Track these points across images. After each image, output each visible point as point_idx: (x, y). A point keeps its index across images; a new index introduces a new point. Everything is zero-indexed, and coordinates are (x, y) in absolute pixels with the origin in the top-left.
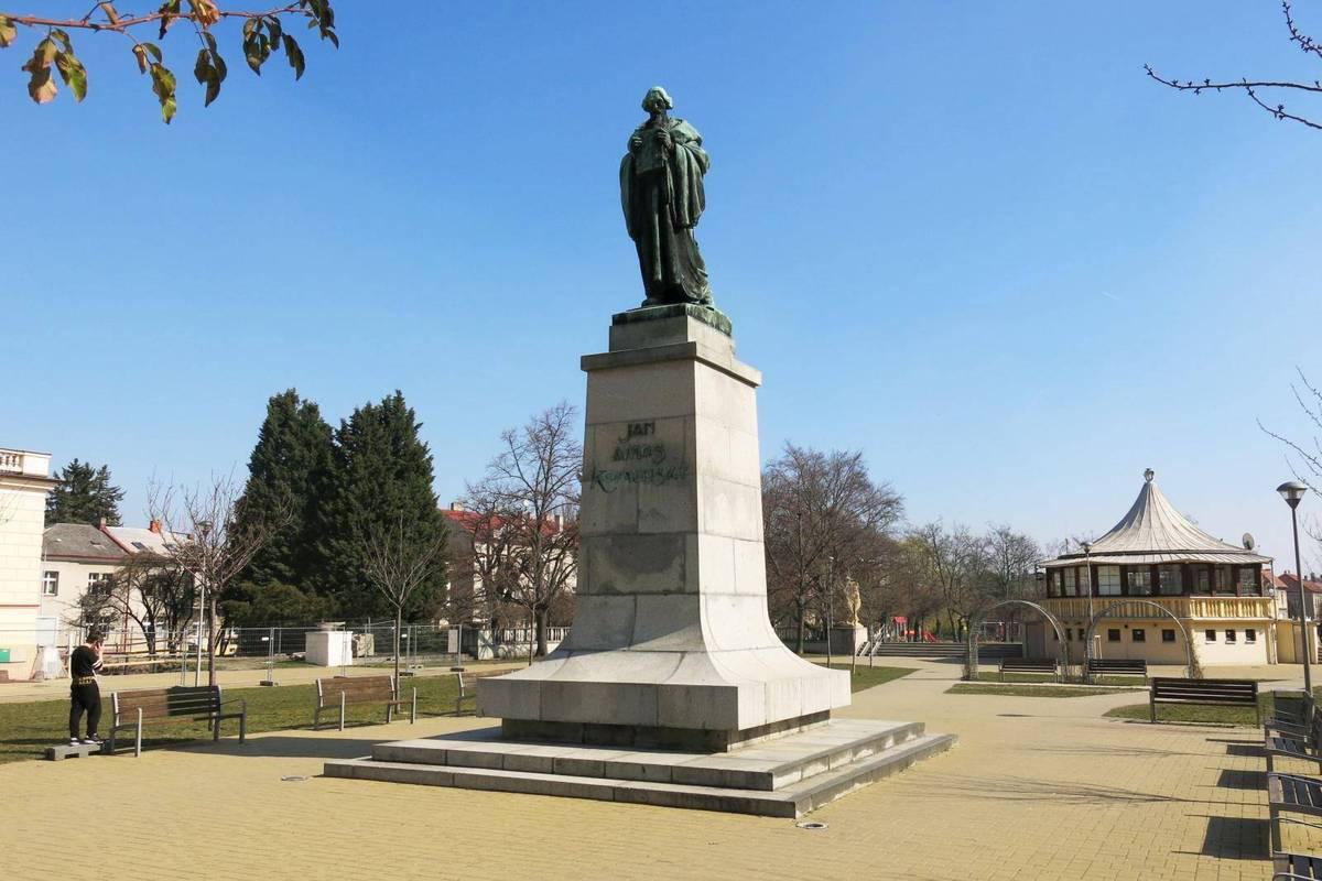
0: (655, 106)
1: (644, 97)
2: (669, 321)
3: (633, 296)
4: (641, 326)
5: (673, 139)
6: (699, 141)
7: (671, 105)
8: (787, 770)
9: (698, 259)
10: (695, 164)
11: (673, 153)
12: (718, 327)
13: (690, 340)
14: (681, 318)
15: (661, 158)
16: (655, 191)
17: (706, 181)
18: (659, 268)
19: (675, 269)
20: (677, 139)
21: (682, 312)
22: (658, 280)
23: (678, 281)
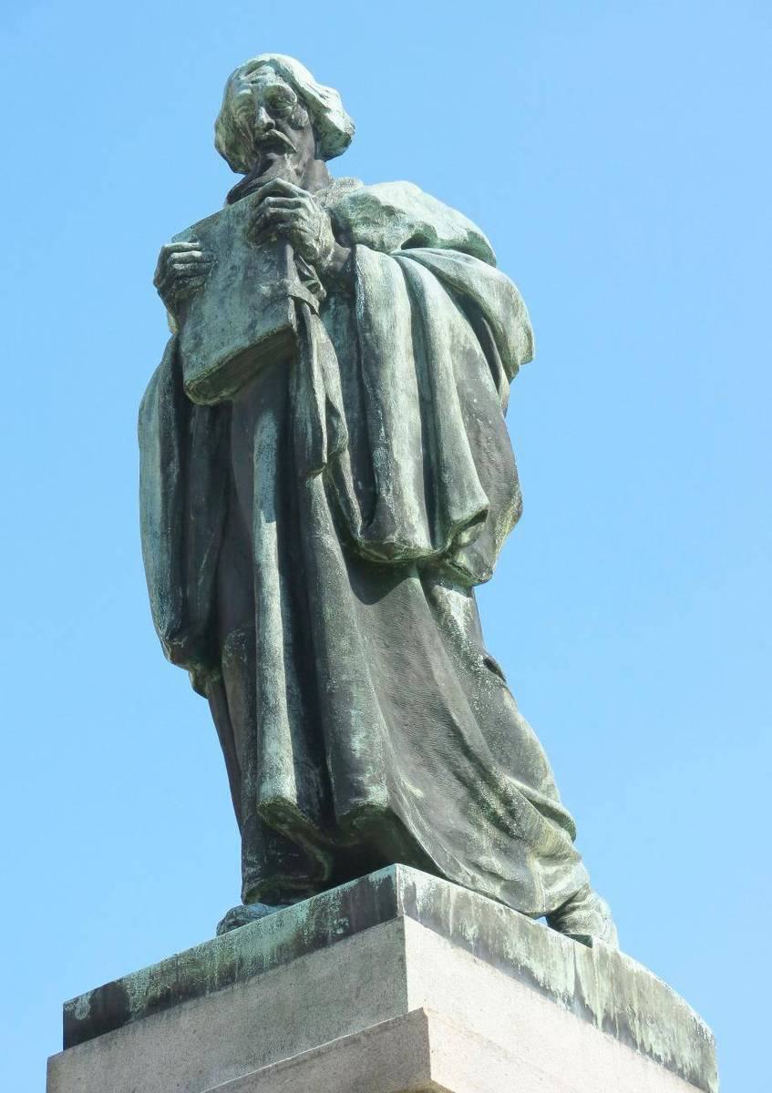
0: (265, 132)
1: (213, 142)
2: (321, 964)
3: (177, 877)
4: (189, 1018)
5: (342, 230)
6: (471, 247)
7: (338, 118)
8: (420, 312)
9: (503, 733)
10: (445, 315)
11: (341, 286)
12: (618, 1026)
13: (412, 1006)
14: (375, 937)
15: (280, 296)
16: (266, 432)
17: (524, 404)
18: (281, 746)
19: (357, 744)
20: (361, 231)
21: (384, 909)
22: (279, 804)
23: (378, 795)
